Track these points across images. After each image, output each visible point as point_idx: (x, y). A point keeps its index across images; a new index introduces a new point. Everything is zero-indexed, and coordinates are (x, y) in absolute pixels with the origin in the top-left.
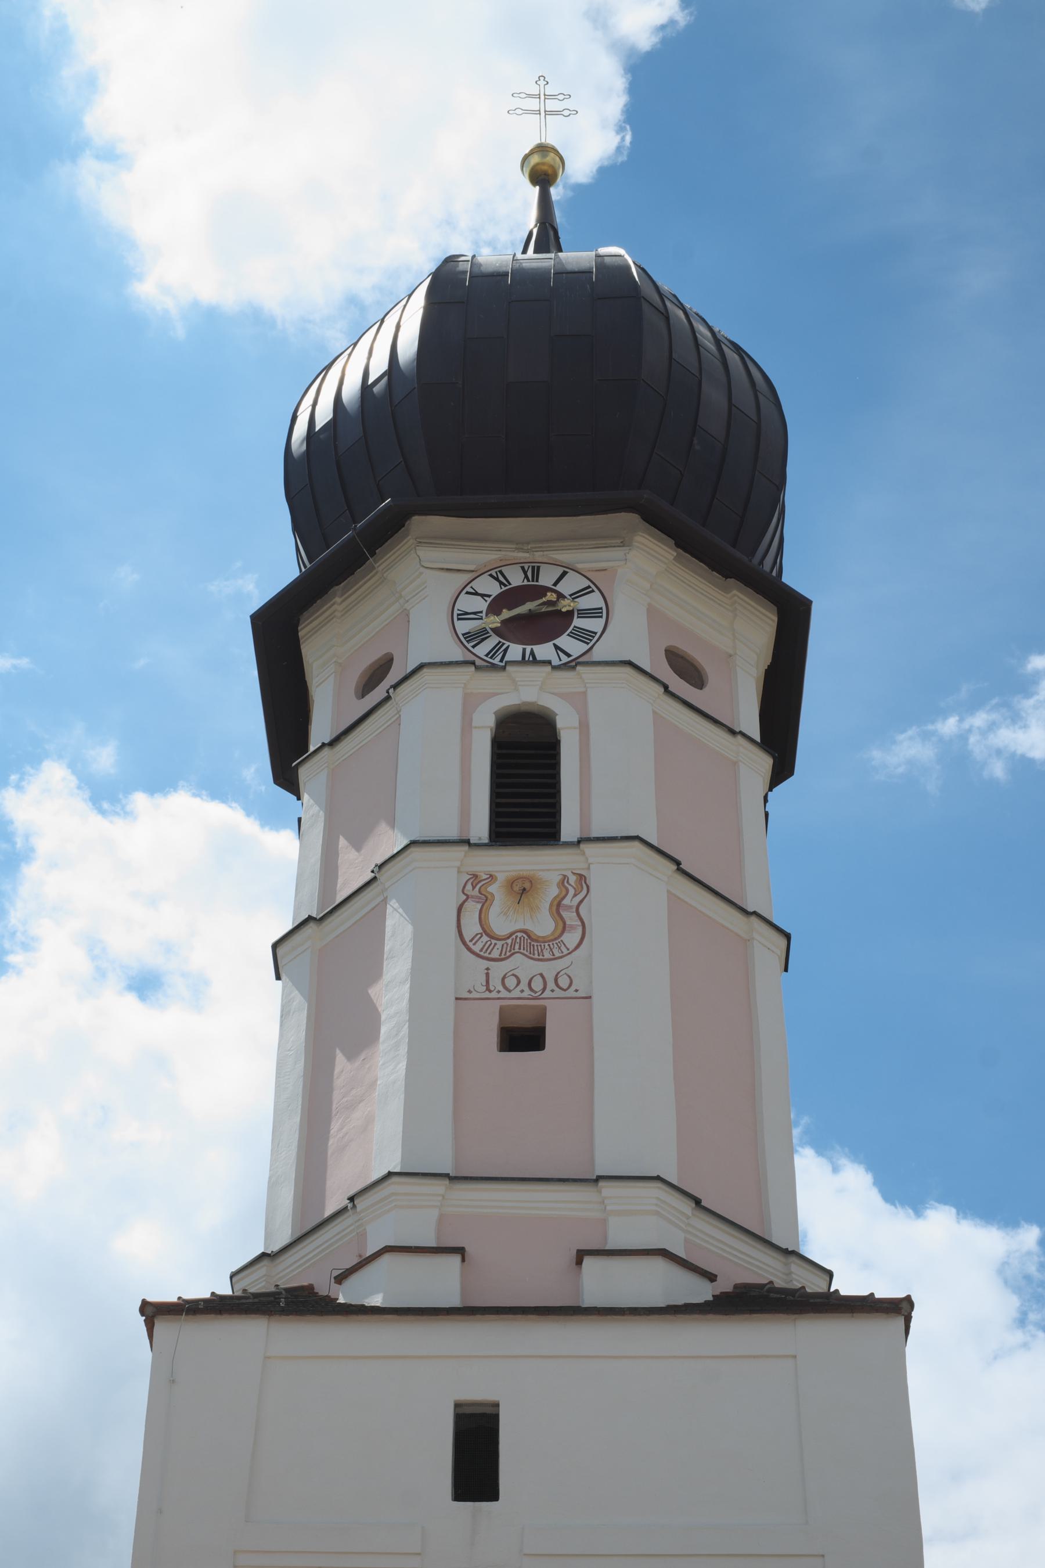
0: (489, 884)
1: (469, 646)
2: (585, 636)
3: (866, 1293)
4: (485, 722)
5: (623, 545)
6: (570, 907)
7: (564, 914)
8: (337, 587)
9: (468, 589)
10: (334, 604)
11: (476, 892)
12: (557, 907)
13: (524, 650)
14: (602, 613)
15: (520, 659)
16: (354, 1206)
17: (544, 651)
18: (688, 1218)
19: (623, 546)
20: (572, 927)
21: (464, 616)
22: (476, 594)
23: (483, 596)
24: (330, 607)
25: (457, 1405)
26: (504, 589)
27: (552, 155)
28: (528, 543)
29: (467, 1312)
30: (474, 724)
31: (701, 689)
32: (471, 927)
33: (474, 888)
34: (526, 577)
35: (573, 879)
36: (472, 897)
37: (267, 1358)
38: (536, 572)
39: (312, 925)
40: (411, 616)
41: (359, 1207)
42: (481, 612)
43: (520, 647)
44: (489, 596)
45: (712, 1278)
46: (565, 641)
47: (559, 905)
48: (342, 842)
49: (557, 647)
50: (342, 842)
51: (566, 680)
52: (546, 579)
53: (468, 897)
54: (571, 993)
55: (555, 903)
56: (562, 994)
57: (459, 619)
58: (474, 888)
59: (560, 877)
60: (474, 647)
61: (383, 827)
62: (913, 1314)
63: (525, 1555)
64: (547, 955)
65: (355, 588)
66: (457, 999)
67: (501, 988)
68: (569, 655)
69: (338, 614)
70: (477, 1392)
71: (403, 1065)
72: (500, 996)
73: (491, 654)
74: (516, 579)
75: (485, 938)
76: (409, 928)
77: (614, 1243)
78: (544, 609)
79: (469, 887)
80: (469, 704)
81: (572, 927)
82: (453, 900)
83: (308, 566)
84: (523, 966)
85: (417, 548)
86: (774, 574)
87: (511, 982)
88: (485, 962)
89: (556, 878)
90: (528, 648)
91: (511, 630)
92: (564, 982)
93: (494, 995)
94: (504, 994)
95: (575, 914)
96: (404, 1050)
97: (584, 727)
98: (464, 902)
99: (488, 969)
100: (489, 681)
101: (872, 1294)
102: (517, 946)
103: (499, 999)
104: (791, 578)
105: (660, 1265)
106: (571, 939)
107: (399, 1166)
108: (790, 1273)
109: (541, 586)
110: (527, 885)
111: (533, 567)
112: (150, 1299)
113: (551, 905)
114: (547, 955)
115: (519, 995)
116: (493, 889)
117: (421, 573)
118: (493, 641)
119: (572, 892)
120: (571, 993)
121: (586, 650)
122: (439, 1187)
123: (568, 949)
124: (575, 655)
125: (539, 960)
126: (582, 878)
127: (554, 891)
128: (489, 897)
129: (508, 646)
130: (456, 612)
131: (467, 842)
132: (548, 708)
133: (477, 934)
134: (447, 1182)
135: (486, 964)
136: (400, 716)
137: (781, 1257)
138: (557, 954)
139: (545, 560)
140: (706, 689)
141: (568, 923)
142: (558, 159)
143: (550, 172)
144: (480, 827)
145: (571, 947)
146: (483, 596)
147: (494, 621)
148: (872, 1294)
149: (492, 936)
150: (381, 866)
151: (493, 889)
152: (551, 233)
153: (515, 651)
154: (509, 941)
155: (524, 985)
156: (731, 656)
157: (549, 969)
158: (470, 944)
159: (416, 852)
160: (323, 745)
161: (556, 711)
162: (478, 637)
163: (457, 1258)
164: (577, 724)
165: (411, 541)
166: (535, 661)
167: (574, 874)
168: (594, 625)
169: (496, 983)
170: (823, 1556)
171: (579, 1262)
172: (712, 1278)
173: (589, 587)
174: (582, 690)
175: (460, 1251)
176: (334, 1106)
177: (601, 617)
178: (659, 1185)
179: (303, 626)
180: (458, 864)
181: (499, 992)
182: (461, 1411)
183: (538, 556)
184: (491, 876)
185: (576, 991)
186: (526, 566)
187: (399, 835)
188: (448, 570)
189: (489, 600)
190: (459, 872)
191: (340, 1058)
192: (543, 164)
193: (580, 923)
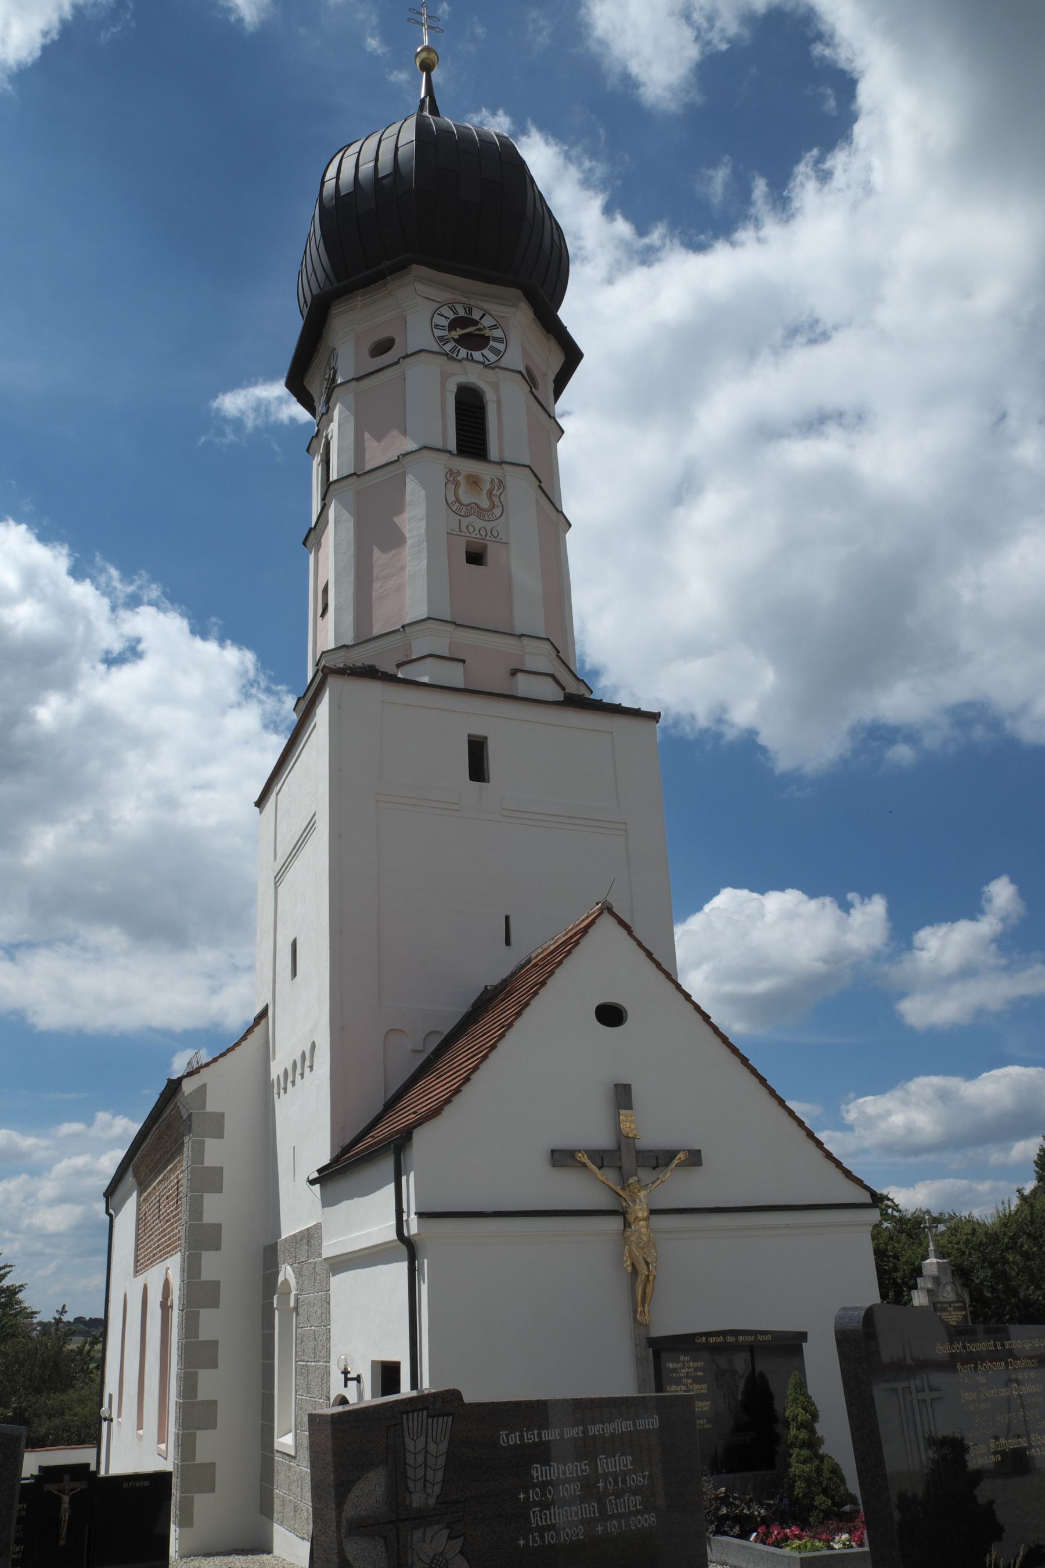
3: (637, 708)
5: (513, 306)
6: (497, 496)
7: (494, 499)
8: (358, 292)
10: (357, 300)
11: (452, 479)
12: (490, 494)
13: (468, 352)
16: (404, 630)
17: (477, 355)
23: (446, 317)
26: (466, 315)
27: (434, 54)
33: (451, 477)
34: (466, 312)
35: (496, 481)
37: (382, 702)
39: (355, 477)
44: (449, 318)
46: (486, 352)
47: (491, 493)
48: (367, 435)
50: (367, 435)
52: (476, 315)
53: (448, 480)
54: (498, 539)
55: (489, 492)
56: (494, 539)
58: (451, 477)
59: (490, 479)
60: (443, 345)
61: (395, 433)
63: (504, 809)
64: (487, 518)
65: (371, 295)
68: (489, 361)
70: (479, 731)
71: (425, 563)
72: (465, 535)
74: (462, 313)
75: (457, 504)
76: (423, 492)
77: (528, 667)
78: (477, 332)
79: (448, 476)
80: (444, 377)
87: (471, 529)
88: (458, 516)
90: (470, 352)
91: (463, 341)
92: (495, 533)
93: (463, 534)
94: (468, 534)
96: (424, 555)
97: (499, 403)
101: (640, 708)
102: (473, 511)
106: (497, 512)
109: (473, 319)
110: (475, 480)
113: (487, 493)
114: (487, 518)
116: (460, 478)
117: (416, 297)
118: (452, 344)
119: (496, 488)
120: (498, 539)
121: (495, 360)
123: (496, 517)
124: (492, 361)
125: (482, 519)
129: (459, 349)
132: (481, 388)
133: (454, 501)
134: (454, 626)
136: (405, 374)
137: (576, 681)
141: (495, 503)
142: (436, 57)
145: (498, 516)
147: (456, 334)
148: (640, 708)
149: (461, 504)
150: (404, 455)
151: (460, 478)
153: (463, 353)
154: (469, 508)
155: (477, 531)
157: (489, 526)
158: (451, 506)
159: (425, 453)
163: (461, 665)
166: (473, 360)
167: (497, 479)
168: (500, 347)
169: (464, 528)
173: (496, 325)
175: (463, 661)
176: (374, 575)
179: (335, 308)
181: (465, 533)
183: (472, 302)
184: (458, 471)
185: (501, 539)
186: (465, 306)
187: (410, 440)
188: (428, 299)
189: (449, 320)
191: (376, 552)
193: (500, 504)
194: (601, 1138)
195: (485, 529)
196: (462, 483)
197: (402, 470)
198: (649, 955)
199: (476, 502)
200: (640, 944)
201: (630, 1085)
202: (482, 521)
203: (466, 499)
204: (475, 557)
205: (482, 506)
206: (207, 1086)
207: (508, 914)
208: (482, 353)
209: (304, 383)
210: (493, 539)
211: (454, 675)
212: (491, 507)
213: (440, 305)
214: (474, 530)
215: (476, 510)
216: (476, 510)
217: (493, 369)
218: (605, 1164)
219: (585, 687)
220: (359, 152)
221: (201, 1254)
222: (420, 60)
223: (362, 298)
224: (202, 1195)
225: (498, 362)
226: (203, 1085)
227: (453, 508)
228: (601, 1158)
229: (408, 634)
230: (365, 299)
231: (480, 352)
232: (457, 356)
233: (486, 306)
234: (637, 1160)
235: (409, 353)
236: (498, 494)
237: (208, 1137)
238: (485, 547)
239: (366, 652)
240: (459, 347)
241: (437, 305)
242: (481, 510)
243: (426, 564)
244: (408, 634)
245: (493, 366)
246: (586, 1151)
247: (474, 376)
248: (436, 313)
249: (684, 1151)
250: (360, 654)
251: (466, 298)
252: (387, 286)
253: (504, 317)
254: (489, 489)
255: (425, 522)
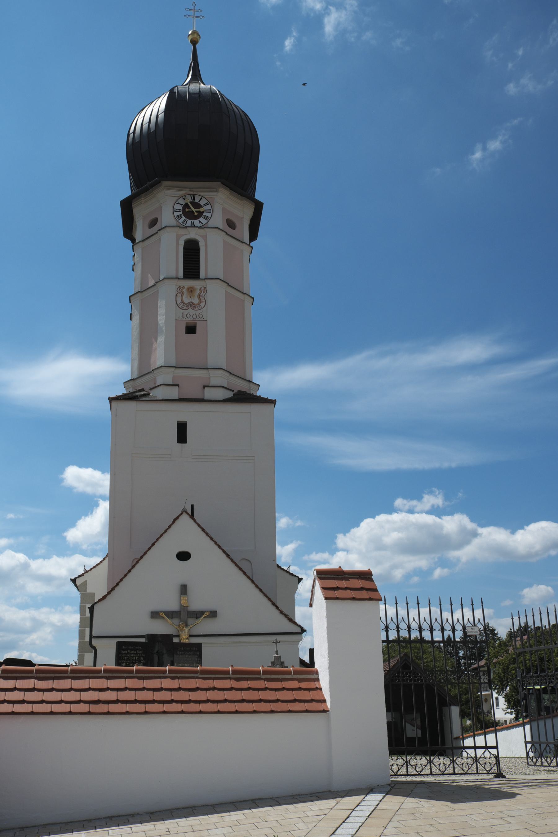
0: (183, 289)
1: (177, 220)
2: (207, 218)
4: (182, 243)
6: (202, 296)
7: (201, 298)
8: (142, 195)
9: (177, 202)
10: (141, 200)
12: (199, 296)
13: (191, 222)
14: (211, 211)
15: (190, 226)
17: (196, 222)
18: (228, 376)
19: (216, 191)
20: (203, 301)
21: (176, 210)
22: (179, 204)
23: (181, 204)
24: (140, 200)
25: (178, 422)
28: (192, 188)
29: (181, 400)
30: (179, 244)
31: (234, 230)
32: (179, 301)
33: (179, 290)
34: (192, 199)
35: (203, 288)
36: (179, 292)
38: (194, 197)
39: (139, 293)
40: (162, 208)
41: (155, 373)
42: (180, 209)
43: (190, 221)
44: (182, 205)
45: (233, 391)
46: (201, 219)
47: (200, 295)
49: (199, 221)
51: (202, 232)
57: (175, 211)
58: (179, 290)
59: (200, 288)
60: (179, 220)
62: (276, 403)
66: (176, 320)
67: (186, 317)
69: (143, 203)
70: (182, 419)
72: (186, 319)
73: (183, 222)
75: (182, 304)
77: (212, 384)
79: (178, 289)
81: (203, 301)
82: (175, 292)
83: (136, 191)
84: (191, 311)
85: (164, 190)
86: (252, 196)
87: (188, 316)
89: (199, 288)
90: (192, 221)
92: (201, 316)
93: (184, 319)
95: (203, 298)
98: (177, 294)
99: (183, 312)
100: (182, 231)
103: (185, 320)
104: (257, 197)
105: (221, 390)
106: (202, 305)
107: (163, 364)
108: (250, 386)
110: (192, 290)
111: (193, 196)
112: (110, 397)
113: (198, 295)
114: (197, 309)
115: (190, 320)
119: (203, 292)
120: (202, 319)
122: (173, 369)
124: (204, 224)
126: (205, 288)
127: (198, 292)
128: (183, 293)
130: (174, 209)
131: (178, 278)
135: (182, 311)
136: (160, 238)
137: (248, 382)
138: (199, 309)
139: (196, 194)
140: (236, 230)
143: (196, 40)
144: (181, 274)
146: (181, 204)
152: (197, 64)
154: (188, 305)
155: (191, 317)
156: (242, 218)
157: (197, 313)
158: (179, 305)
160: (140, 241)
161: (200, 241)
162: (179, 217)
163: (177, 387)
164: (204, 245)
165: (163, 188)
168: (209, 215)
169: (185, 316)
170: (254, 457)
171: (204, 388)
172: (233, 391)
173: (208, 203)
174: (206, 234)
175: (178, 385)
177: (211, 212)
178: (222, 370)
180: (176, 284)
182: (178, 422)
183: (195, 193)
184: (184, 287)
186: (192, 195)
189: (182, 206)
190: (176, 285)
192: (194, 38)
193: (204, 300)
194: (173, 606)
195: (196, 315)
196: (185, 293)
197: (157, 290)
198: (203, 530)
199: (192, 301)
200: (199, 526)
201: (187, 585)
202: (195, 311)
203: (186, 300)
204: (191, 329)
205: (195, 303)
206: (87, 581)
207: (192, 504)
208: (199, 220)
209: (133, 234)
210: (200, 319)
211: (173, 393)
212: (200, 302)
213: (178, 198)
214: (190, 316)
215: (192, 305)
216: (192, 305)
217: (204, 228)
218: (173, 617)
219: (254, 384)
220: (144, 117)
221: (84, 654)
222: (191, 38)
223: (144, 198)
224: (85, 629)
225: (207, 224)
226: (85, 581)
227: (180, 306)
228: (171, 615)
229: (155, 374)
230: (145, 199)
231: (198, 220)
232: (186, 224)
233: (202, 194)
234: (188, 615)
235: (163, 227)
236: (203, 295)
237: (88, 604)
238: (196, 323)
239: (145, 380)
240: (187, 219)
241: (177, 198)
242: (194, 305)
243: (164, 338)
244: (155, 374)
245: (203, 227)
246: (163, 612)
247: (193, 234)
248: (176, 203)
249: (208, 611)
250: (142, 381)
251: (192, 191)
252: (153, 192)
253: (211, 198)
254: (199, 293)
255: (164, 316)
